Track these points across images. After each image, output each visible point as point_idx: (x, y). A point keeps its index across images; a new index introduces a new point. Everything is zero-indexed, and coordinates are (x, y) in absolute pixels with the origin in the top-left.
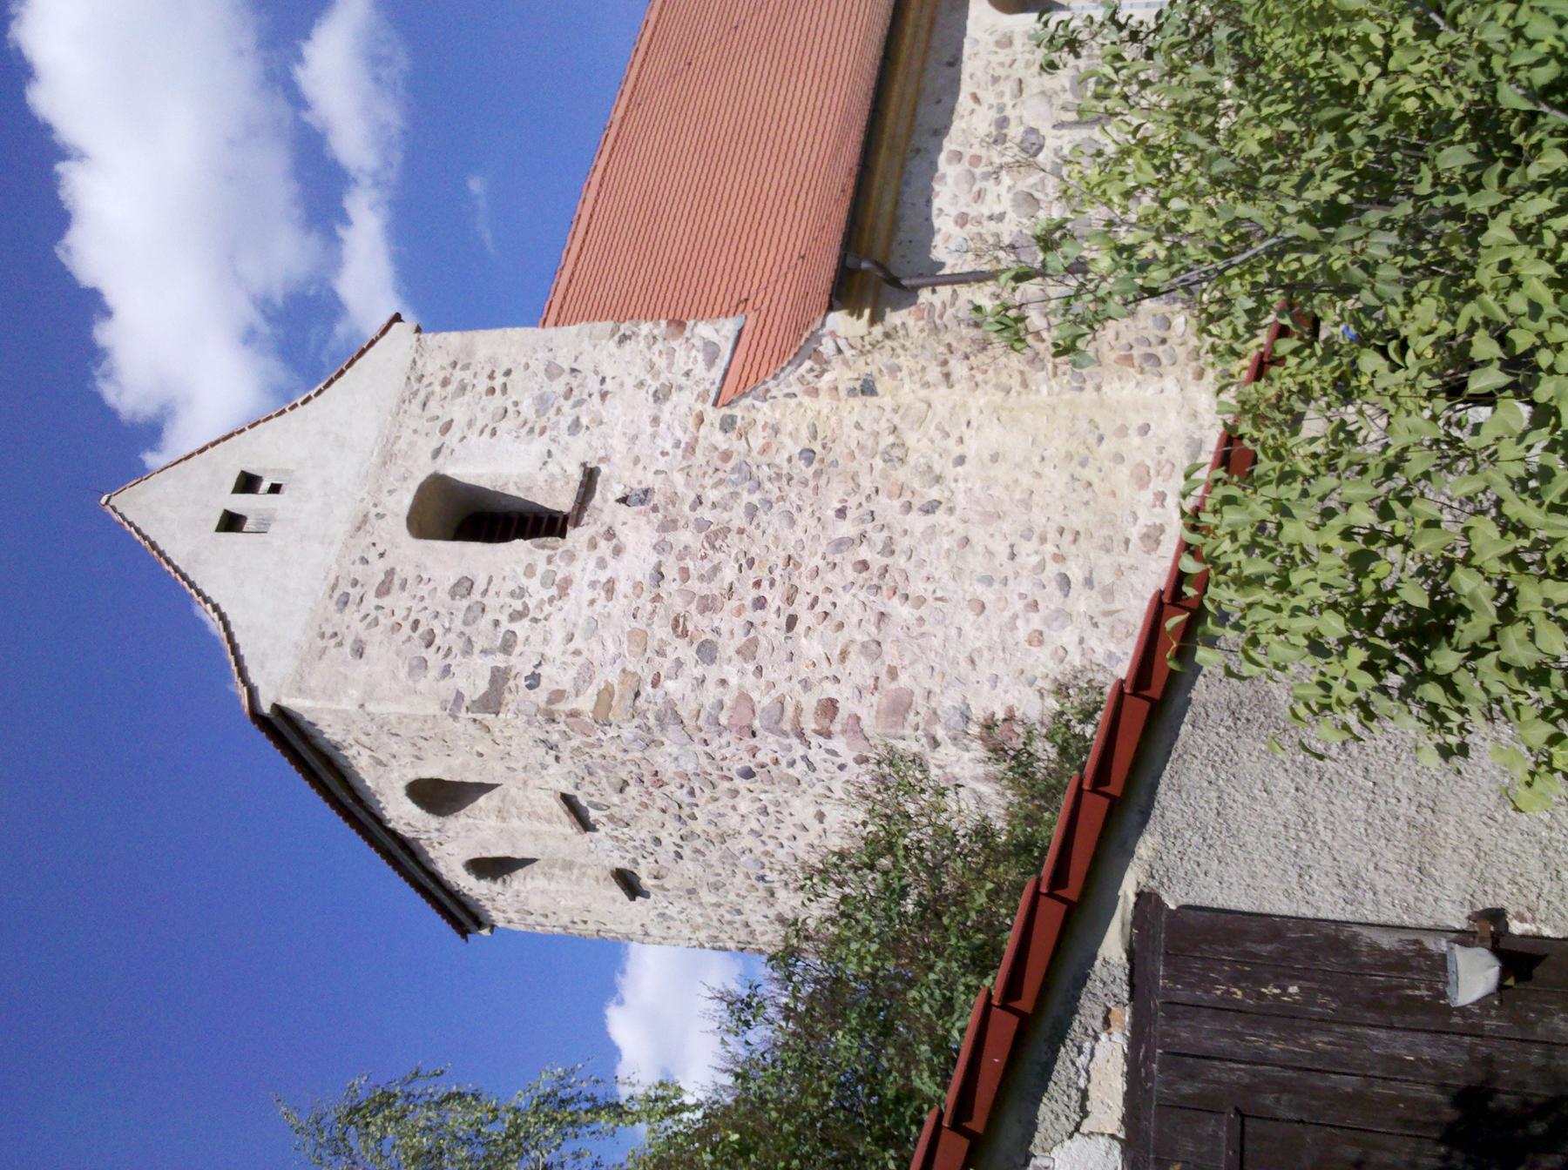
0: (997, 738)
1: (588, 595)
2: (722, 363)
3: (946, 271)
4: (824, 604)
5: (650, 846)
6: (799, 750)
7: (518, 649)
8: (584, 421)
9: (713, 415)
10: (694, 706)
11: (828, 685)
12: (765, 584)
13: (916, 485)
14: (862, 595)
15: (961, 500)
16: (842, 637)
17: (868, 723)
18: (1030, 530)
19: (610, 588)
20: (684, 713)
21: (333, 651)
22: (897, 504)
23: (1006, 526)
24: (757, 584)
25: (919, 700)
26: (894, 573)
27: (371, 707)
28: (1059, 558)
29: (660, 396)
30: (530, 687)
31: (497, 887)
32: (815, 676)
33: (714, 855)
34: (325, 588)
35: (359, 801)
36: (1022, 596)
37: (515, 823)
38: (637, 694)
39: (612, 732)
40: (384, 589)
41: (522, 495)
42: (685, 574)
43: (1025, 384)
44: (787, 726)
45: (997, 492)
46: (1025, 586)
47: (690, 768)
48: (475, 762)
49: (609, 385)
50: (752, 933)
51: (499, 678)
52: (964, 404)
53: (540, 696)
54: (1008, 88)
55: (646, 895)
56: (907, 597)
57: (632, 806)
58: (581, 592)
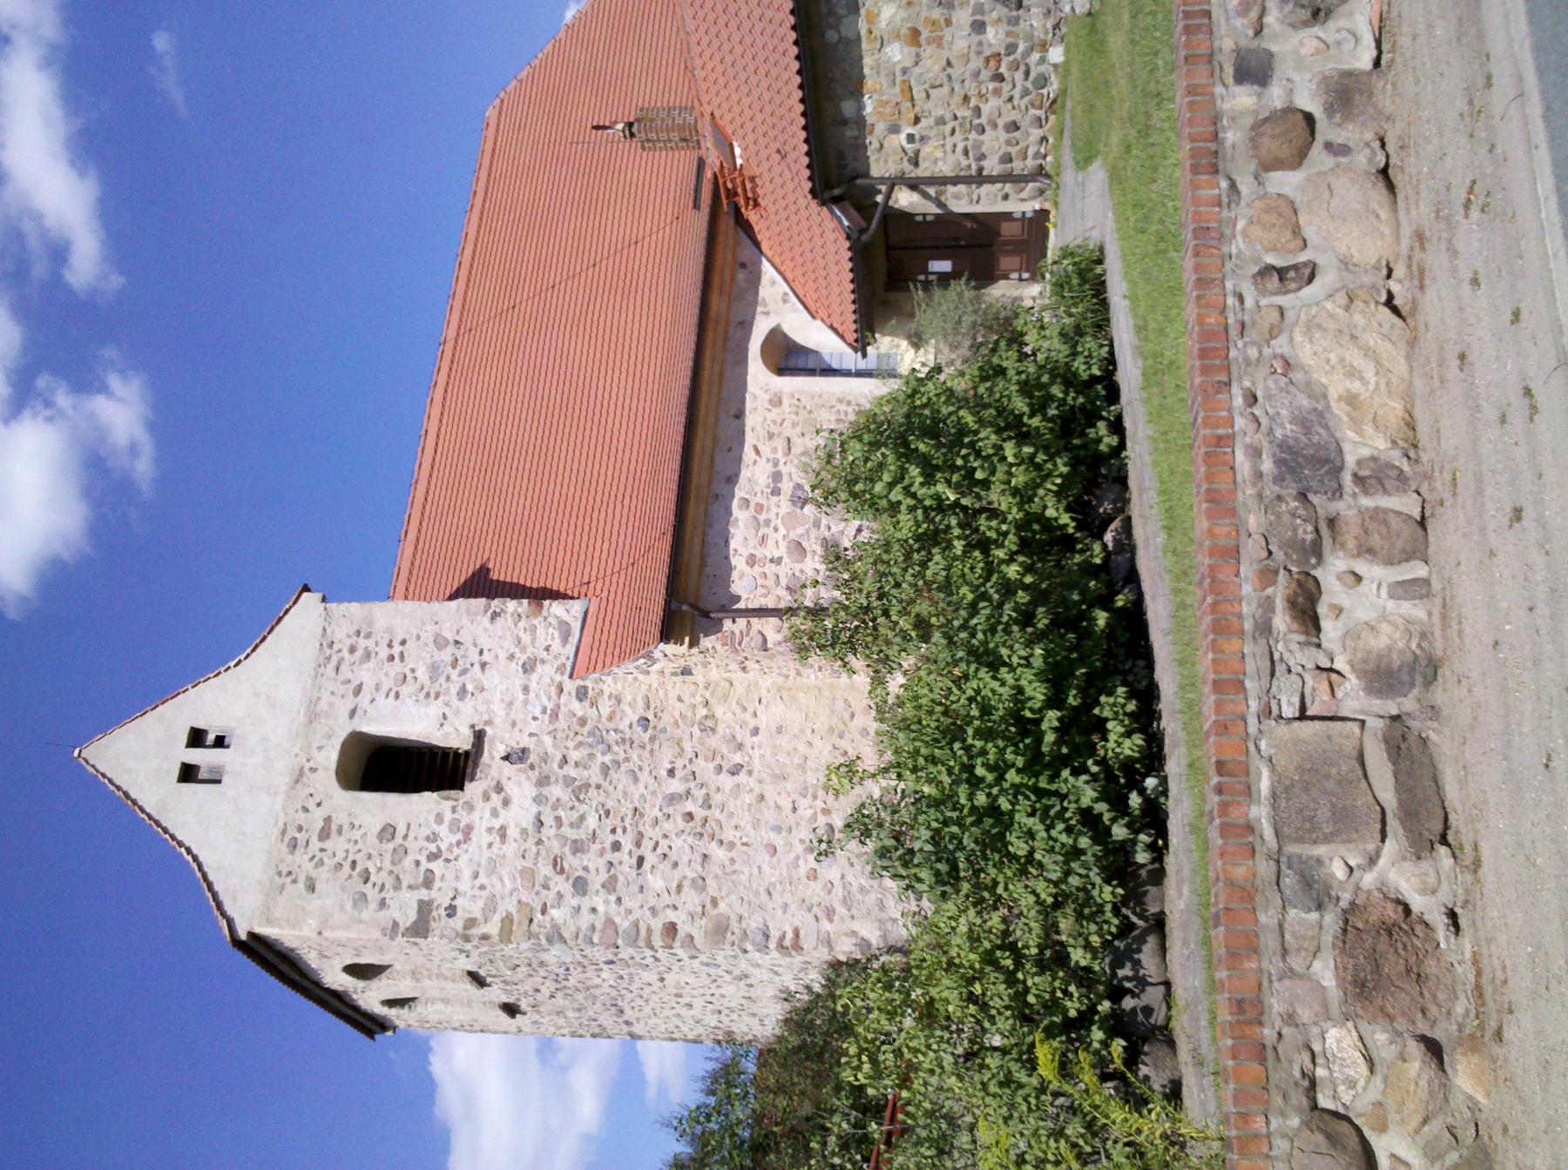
1: (486, 839)
3: (741, 605)
6: (649, 953)
7: (437, 884)
8: (470, 687)
9: (570, 686)
10: (573, 929)
11: (669, 912)
12: (619, 831)
13: (724, 750)
14: (690, 840)
16: (678, 874)
19: (503, 833)
20: (566, 935)
21: (290, 888)
22: (711, 766)
23: (789, 786)
24: (613, 831)
25: (734, 924)
28: (826, 812)
29: (528, 668)
30: (449, 916)
33: (580, 997)
34: (276, 832)
37: (427, 983)
38: (531, 921)
40: (324, 834)
41: (752, 420)
43: (799, 674)
45: (782, 758)
49: (487, 657)
51: (425, 908)
53: (458, 923)
54: (780, 444)
58: (480, 837)
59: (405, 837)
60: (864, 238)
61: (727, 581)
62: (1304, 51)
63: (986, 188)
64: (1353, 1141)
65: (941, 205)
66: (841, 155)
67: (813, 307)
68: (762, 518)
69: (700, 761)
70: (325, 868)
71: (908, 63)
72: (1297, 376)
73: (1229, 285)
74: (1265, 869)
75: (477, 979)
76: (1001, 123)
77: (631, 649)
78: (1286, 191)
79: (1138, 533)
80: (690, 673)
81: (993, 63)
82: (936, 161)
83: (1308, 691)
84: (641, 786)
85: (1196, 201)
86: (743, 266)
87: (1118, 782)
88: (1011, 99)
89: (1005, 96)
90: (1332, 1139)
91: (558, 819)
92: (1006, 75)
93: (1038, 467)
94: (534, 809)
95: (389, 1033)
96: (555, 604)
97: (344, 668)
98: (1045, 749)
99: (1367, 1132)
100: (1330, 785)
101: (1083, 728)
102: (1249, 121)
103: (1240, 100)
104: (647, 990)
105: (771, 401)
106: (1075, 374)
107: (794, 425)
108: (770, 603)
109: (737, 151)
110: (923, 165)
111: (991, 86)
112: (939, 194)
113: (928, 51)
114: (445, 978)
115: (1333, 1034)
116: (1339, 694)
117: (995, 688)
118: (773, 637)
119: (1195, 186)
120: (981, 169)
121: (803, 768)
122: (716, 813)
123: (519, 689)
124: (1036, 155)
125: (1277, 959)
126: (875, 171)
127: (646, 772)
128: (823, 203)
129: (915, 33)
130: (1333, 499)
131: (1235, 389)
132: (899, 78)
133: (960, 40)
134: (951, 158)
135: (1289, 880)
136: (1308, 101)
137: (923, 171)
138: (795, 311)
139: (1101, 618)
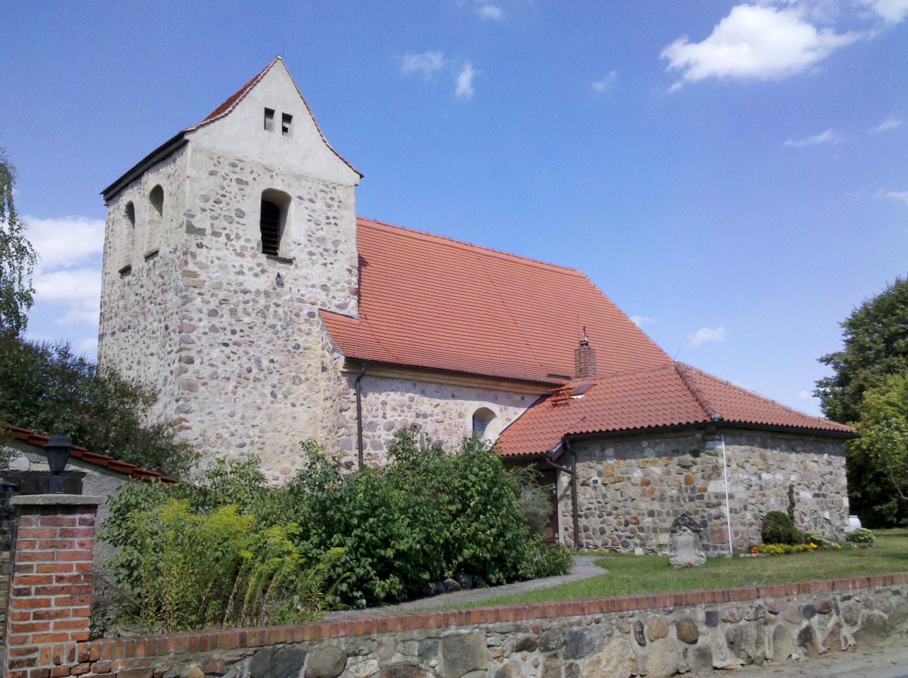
1: (237, 264)
3: (362, 398)
6: (175, 349)
7: (214, 238)
8: (314, 257)
9: (315, 309)
11: (200, 360)
12: (242, 334)
14: (237, 371)
16: (219, 364)
19: (241, 273)
20: (188, 305)
21: (212, 162)
22: (276, 382)
23: (265, 423)
24: (242, 331)
25: (194, 394)
28: (252, 443)
29: (324, 288)
34: (240, 157)
40: (239, 181)
41: (451, 403)
43: (324, 428)
45: (280, 419)
49: (329, 266)
51: (201, 232)
53: (194, 249)
54: (440, 417)
58: (239, 261)
59: (238, 223)
60: (548, 460)
63: (571, 519)
65: (562, 497)
66: (586, 448)
67: (505, 434)
68: (405, 408)
69: (278, 377)
70: (222, 181)
71: (632, 480)
72: (606, 639)
73: (637, 612)
74: (433, 632)
76: (604, 526)
77: (339, 341)
78: (670, 633)
79: (455, 593)
81: (634, 521)
83: (496, 648)
84: (265, 345)
86: (523, 399)
87: (362, 583)
88: (616, 530)
89: (618, 527)
90: (338, 663)
91: (248, 302)
94: (253, 290)
95: (104, 202)
96: (356, 302)
97: (323, 194)
98: (378, 550)
101: (385, 569)
102: (693, 618)
103: (701, 615)
105: (460, 413)
106: (519, 563)
107: (450, 424)
108: (364, 413)
109: (580, 397)
110: (582, 488)
112: (567, 496)
113: (639, 489)
114: (150, 238)
115: (374, 662)
116: (495, 661)
117: (401, 526)
118: (347, 414)
119: (669, 597)
120: (580, 516)
121: (275, 430)
122: (252, 384)
123: (313, 283)
124: (588, 544)
126: (579, 466)
127: (272, 348)
128: (563, 440)
129: (648, 483)
131: (601, 615)
132: (625, 476)
133: (645, 505)
135: (429, 642)
136: (702, 641)
137: (580, 489)
138: (503, 425)
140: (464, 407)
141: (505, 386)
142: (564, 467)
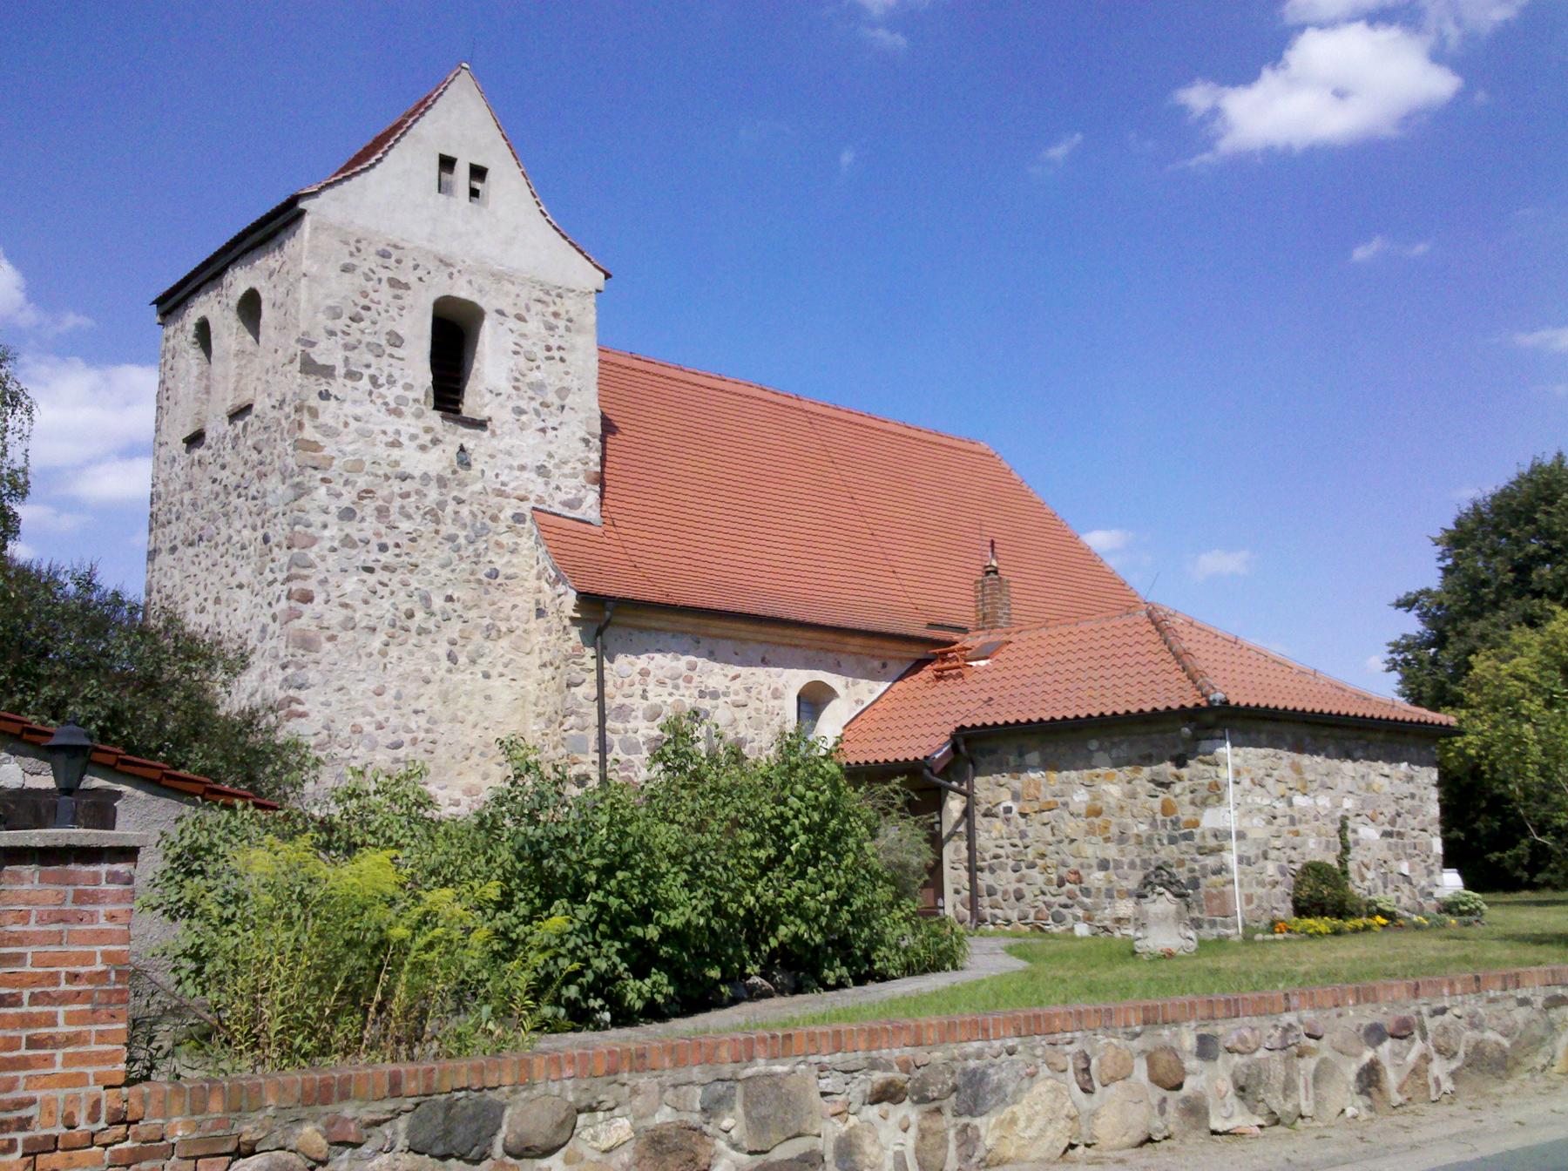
0: (287, 708)
1: (390, 429)
2: (566, 512)
3: (606, 664)
4: (380, 590)
5: (220, 461)
6: (281, 576)
7: (349, 383)
8: (524, 418)
9: (526, 508)
10: (308, 507)
11: (323, 596)
12: (397, 551)
13: (469, 648)
14: (389, 616)
15: (456, 677)
16: (358, 604)
17: (296, 623)
18: (435, 723)
19: (395, 444)
20: (302, 501)
21: (346, 250)
22: (456, 636)
23: (437, 707)
24: (397, 545)
25: (313, 656)
26: (404, 635)
27: (304, 281)
28: (414, 742)
29: (542, 470)
30: (320, 394)
31: (191, 338)
32: (330, 588)
33: (215, 506)
34: (394, 239)
35: (246, 252)
36: (387, 720)
37: (234, 364)
38: (315, 468)
39: (290, 450)
40: (394, 283)
41: (761, 672)
42: (406, 495)
43: (539, 715)
44: (294, 570)
45: (463, 700)
46: (394, 721)
47: (269, 500)
48: (272, 346)
49: (550, 433)
50: (163, 526)
51: (328, 371)
52: (527, 676)
53: (314, 401)
54: (742, 698)
55: (188, 451)
56: (387, 645)
57: (246, 454)
58: (392, 424)
59: (391, 356)
60: (926, 772)
61: (627, 650)
62: (1219, 1082)
63: (965, 875)
64: (560, 1140)
65: (950, 836)
66: (993, 752)
67: (852, 726)
72: (1026, 1083)
73: (1078, 1034)
74: (727, 1070)
75: (240, 412)
76: (1023, 886)
78: (1136, 1072)
80: (538, 616)
81: (1073, 877)
82: (989, 832)
83: (835, 1097)
84: (438, 571)
85: (1127, 1010)
86: (884, 666)
88: (1043, 893)
89: (1045, 889)
90: (561, 1125)
92: (1064, 889)
93: (816, 919)
94: (417, 473)
95: (158, 319)
99: (564, 1150)
100: (780, 1114)
101: (642, 959)
103: (1189, 1041)
104: (225, 572)
107: (757, 710)
108: (609, 689)
109: (983, 663)
110: (985, 821)
111: (1054, 877)
113: (1082, 823)
114: (238, 382)
115: (625, 1123)
116: (834, 1120)
117: (673, 886)
120: (981, 870)
122: (413, 639)
125: (671, 1081)
126: (979, 782)
127: (451, 576)
128: (953, 736)
129: (1098, 813)
130: (953, 1110)
131: (1017, 1040)
133: (1092, 850)
134: (991, 844)
135: (720, 1088)
137: (980, 822)
139: (715, 973)
140: (782, 681)
141: (855, 643)
142: (955, 784)
